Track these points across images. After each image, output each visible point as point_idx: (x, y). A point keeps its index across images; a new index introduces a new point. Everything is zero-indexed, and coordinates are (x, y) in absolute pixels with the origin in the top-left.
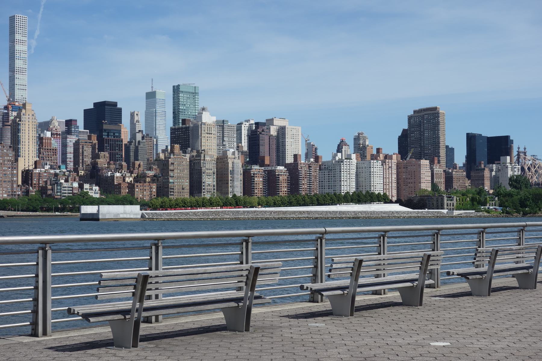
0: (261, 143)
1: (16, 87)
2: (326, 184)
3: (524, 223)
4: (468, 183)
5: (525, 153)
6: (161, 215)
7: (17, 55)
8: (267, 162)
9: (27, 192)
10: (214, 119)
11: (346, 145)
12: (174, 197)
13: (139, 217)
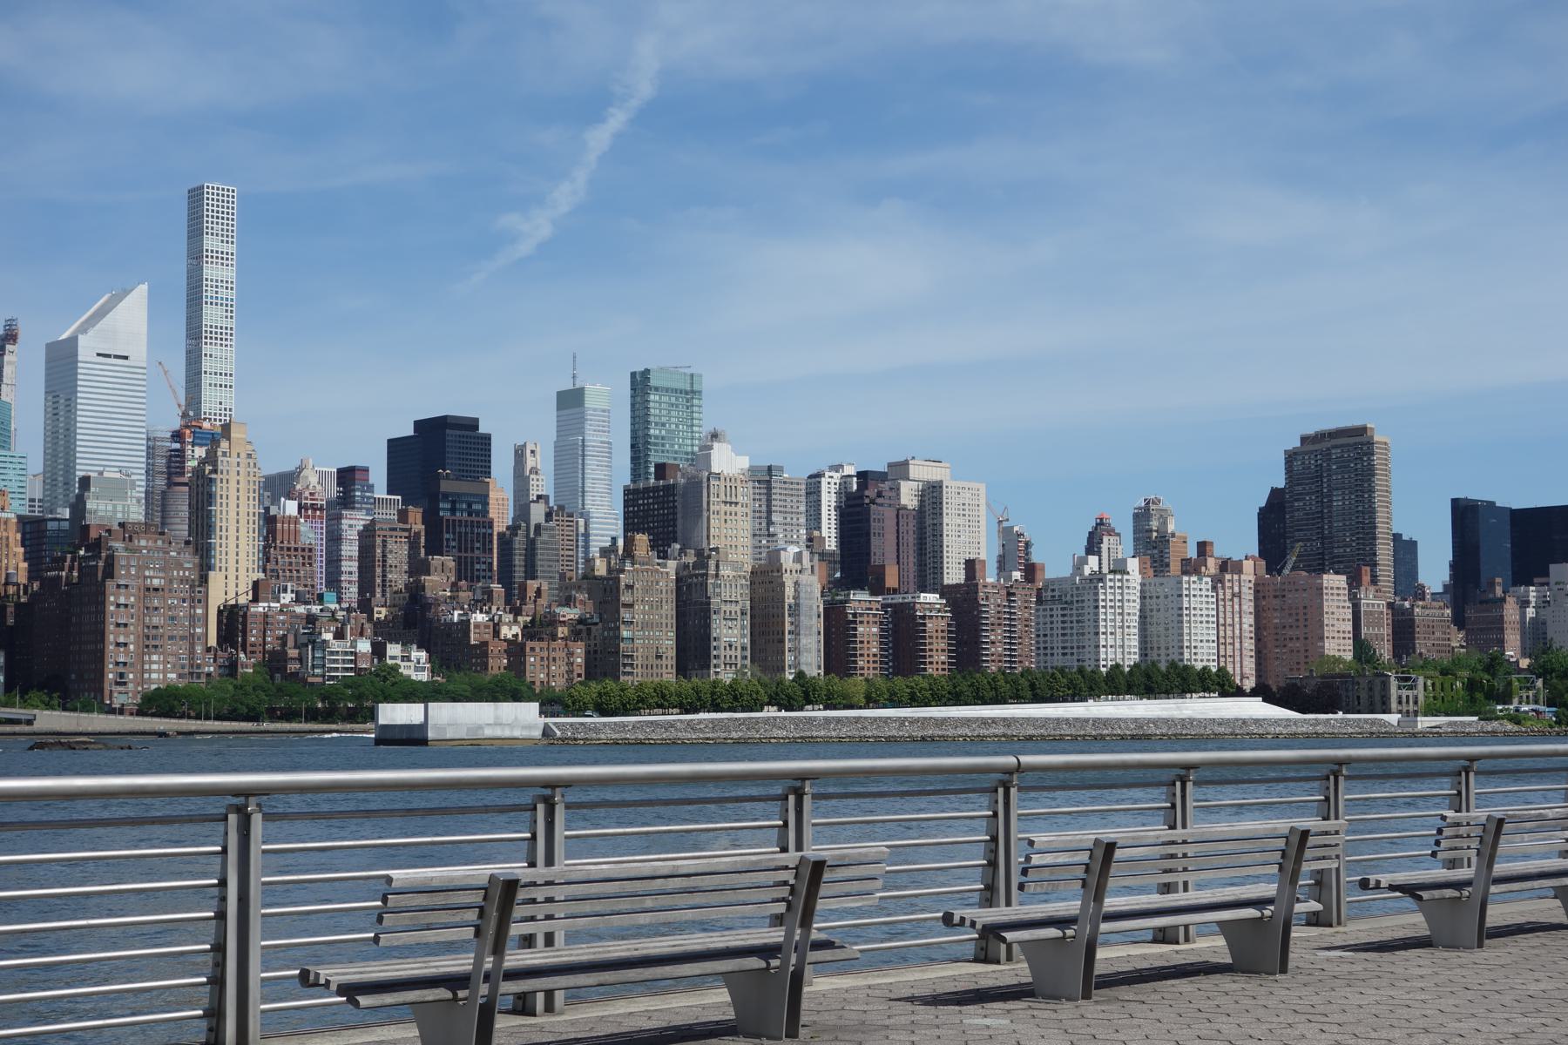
0: (874, 528)
1: (206, 380)
2: (1058, 643)
4: (1457, 639)
7: (208, 292)
8: (891, 580)
9: (232, 667)
10: (744, 463)
11: (1111, 532)
12: (632, 679)
13: (537, 733)
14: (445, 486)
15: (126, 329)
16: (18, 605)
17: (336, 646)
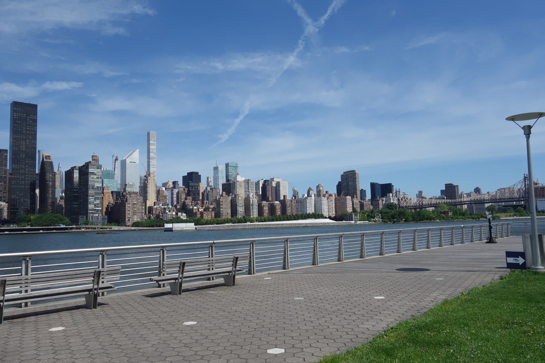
0: (268, 190)
1: (151, 166)
2: (300, 210)
3: (342, 233)
4: (371, 207)
5: (399, 192)
6: (205, 228)
7: (151, 151)
8: (270, 199)
9: (150, 217)
10: (244, 179)
11: (312, 190)
12: (224, 217)
13: (194, 229)
14: (190, 184)
15: (135, 158)
16: (111, 207)
17: (169, 213)
